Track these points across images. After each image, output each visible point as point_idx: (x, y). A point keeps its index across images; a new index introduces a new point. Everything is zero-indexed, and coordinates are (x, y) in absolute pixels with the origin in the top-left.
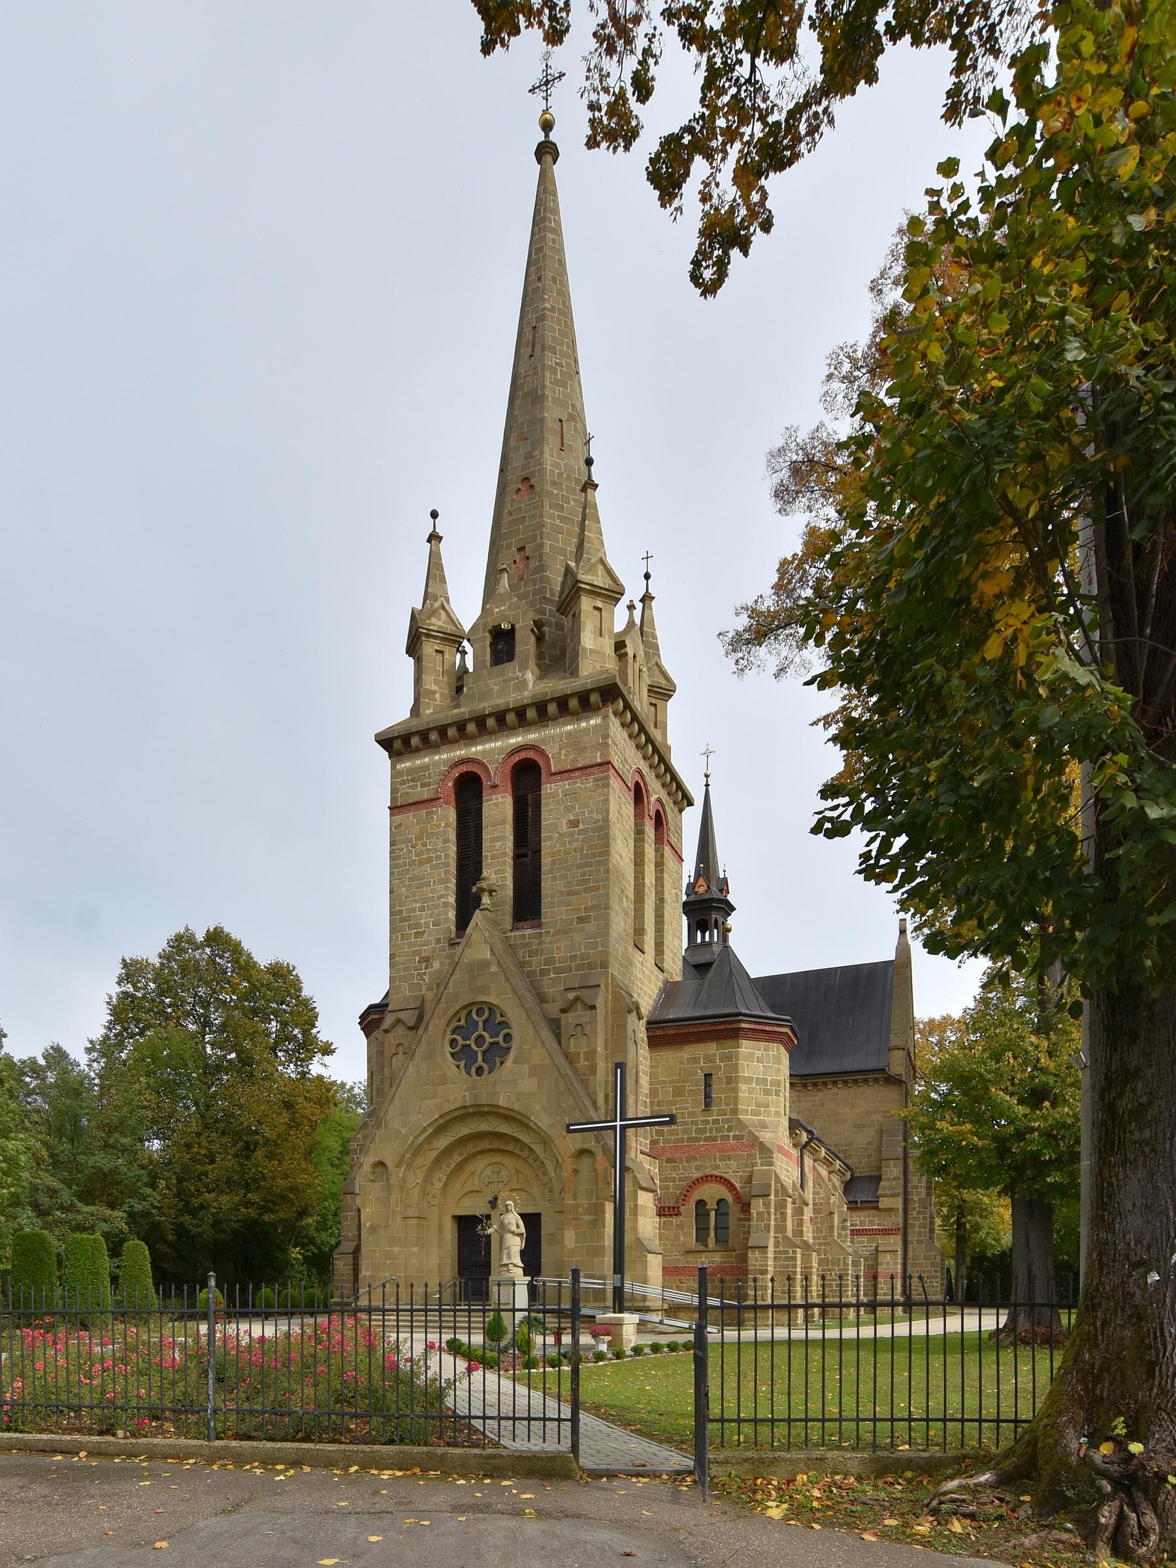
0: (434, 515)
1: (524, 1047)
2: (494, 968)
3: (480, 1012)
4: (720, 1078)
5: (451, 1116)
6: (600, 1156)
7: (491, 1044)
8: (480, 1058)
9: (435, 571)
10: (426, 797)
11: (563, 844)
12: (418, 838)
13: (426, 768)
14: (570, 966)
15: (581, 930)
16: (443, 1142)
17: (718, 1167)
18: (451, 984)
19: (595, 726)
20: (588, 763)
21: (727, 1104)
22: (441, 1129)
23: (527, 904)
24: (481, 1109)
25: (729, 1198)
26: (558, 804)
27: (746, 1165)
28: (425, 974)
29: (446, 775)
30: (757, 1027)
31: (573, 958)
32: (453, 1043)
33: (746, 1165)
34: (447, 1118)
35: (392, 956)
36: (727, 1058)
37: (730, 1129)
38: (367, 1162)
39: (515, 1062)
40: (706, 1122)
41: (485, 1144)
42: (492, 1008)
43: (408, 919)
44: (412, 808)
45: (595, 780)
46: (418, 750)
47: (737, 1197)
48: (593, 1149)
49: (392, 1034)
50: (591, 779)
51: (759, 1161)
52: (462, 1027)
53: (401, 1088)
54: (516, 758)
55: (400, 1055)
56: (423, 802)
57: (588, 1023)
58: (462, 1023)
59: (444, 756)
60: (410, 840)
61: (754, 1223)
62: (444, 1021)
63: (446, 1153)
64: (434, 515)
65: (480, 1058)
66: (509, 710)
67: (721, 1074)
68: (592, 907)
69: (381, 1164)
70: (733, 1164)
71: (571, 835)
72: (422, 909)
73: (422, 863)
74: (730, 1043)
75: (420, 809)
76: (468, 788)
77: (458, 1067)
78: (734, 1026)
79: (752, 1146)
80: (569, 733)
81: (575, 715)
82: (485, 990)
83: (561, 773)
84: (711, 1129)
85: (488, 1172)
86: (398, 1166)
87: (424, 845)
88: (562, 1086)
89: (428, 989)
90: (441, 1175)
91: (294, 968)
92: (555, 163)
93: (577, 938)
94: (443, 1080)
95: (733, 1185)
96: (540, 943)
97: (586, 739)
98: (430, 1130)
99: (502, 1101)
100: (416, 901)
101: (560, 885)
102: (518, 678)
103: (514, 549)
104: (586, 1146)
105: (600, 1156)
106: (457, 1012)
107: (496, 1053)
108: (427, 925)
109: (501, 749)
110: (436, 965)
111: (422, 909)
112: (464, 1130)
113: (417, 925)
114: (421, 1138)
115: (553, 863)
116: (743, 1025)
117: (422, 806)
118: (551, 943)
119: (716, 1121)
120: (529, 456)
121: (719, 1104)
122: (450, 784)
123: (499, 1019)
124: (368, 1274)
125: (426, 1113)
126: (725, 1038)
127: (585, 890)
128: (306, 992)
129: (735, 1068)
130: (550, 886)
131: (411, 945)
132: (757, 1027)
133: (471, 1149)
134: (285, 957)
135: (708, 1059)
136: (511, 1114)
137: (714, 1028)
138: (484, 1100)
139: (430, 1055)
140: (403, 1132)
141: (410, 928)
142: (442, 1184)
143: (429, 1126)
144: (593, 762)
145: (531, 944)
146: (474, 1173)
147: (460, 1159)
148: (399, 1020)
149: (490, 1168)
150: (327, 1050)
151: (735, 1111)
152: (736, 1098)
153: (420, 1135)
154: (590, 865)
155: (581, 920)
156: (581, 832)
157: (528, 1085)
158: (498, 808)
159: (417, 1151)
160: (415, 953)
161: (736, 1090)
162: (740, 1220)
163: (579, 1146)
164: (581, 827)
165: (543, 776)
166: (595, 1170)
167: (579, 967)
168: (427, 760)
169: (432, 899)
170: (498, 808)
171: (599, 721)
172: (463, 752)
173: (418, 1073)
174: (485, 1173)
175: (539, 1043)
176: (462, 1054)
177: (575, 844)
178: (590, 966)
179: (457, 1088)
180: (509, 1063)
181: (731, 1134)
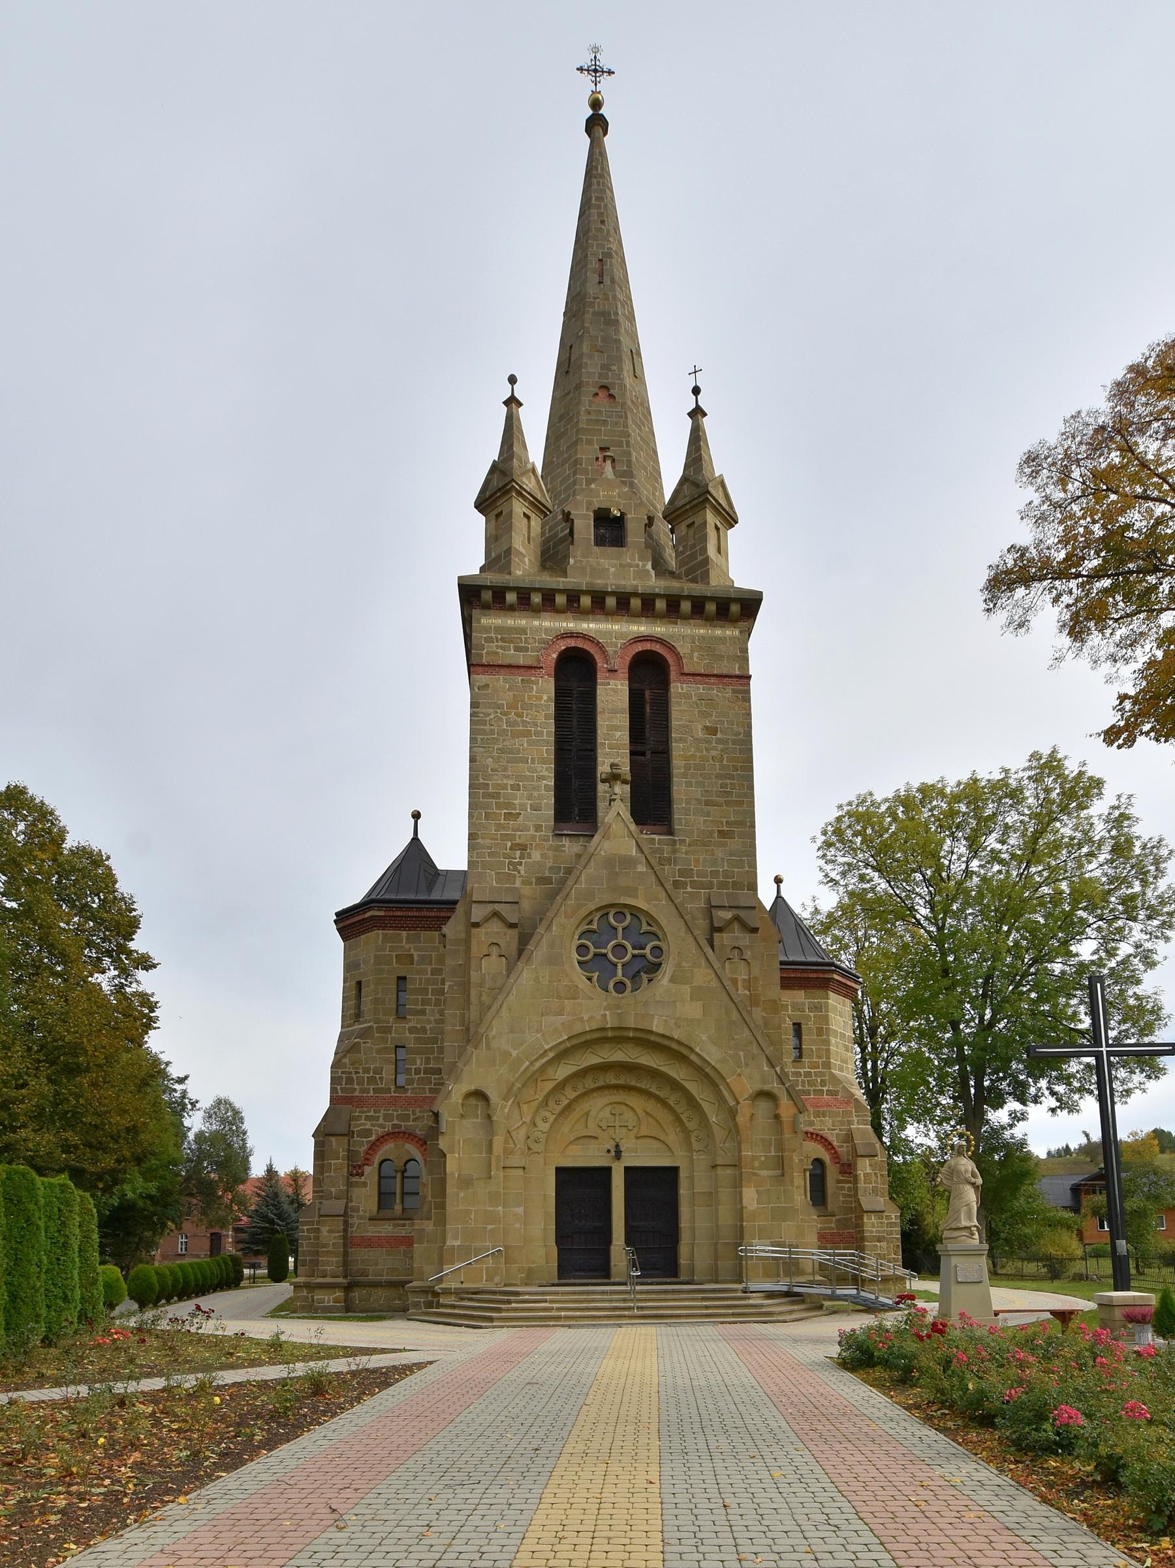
0: (512, 380)
1: (684, 964)
2: (642, 868)
3: (620, 915)
4: (810, 1029)
5: (583, 1039)
6: (784, 1100)
7: (634, 956)
8: (620, 972)
9: (512, 432)
10: (521, 662)
11: (698, 749)
12: (510, 706)
13: (523, 631)
14: (711, 883)
15: (724, 845)
16: (563, 1071)
17: (812, 1123)
18: (583, 877)
19: (732, 638)
20: (725, 672)
21: (819, 1057)
22: (563, 1054)
23: (652, 804)
24: (626, 1034)
25: (827, 1158)
26: (691, 706)
27: (842, 1123)
28: (521, 864)
29: (549, 645)
30: (843, 980)
31: (714, 874)
32: (582, 950)
33: (842, 1123)
34: (575, 1042)
35: (472, 837)
36: (817, 1008)
37: (823, 1083)
38: (457, 1090)
39: (673, 980)
40: (798, 1074)
41: (611, 1079)
42: (636, 912)
43: (496, 796)
44: (502, 670)
45: (734, 691)
46: (512, 608)
47: (836, 1156)
48: (775, 1091)
49: (482, 930)
50: (729, 689)
51: (855, 1119)
52: (594, 932)
53: (511, 997)
54: (640, 647)
55: (494, 957)
56: (519, 667)
57: (747, 947)
58: (595, 926)
59: (546, 624)
60: (500, 707)
61: (861, 1185)
62: (574, 921)
63: (561, 1086)
64: (512, 380)
65: (620, 972)
66: (635, 594)
67: (811, 1024)
68: (736, 823)
69: (479, 1095)
70: (829, 1121)
71: (708, 742)
72: (515, 787)
73: (516, 735)
74: (819, 992)
75: (513, 674)
76: (576, 669)
77: (590, 979)
78: (826, 976)
79: (848, 1103)
80: (703, 638)
81: (709, 620)
82: (632, 891)
83: (694, 675)
84: (803, 1082)
85: (606, 1113)
86: (506, 1099)
87: (520, 715)
88: (735, 1015)
89: (523, 882)
90: (548, 1114)
91: (108, 858)
92: (605, 133)
93: (719, 853)
94: (573, 993)
95: (830, 1144)
96: (674, 851)
97: (722, 647)
98: (551, 1055)
99: (657, 1026)
100: (507, 777)
101: (697, 792)
102: (638, 566)
103: (597, 447)
104: (766, 1087)
105: (784, 1100)
106: (591, 913)
107: (647, 968)
108: (523, 807)
109: (619, 635)
110: (536, 856)
111: (515, 787)
112: (591, 1059)
113: (508, 805)
114: (538, 1065)
115: (688, 767)
116: (836, 977)
117: (515, 671)
118: (686, 853)
119: (808, 1074)
120: (606, 367)
121: (811, 1056)
122: (555, 656)
123: (645, 928)
124: (457, 1243)
125: (551, 1031)
126: (815, 987)
127: (727, 803)
128: (124, 887)
129: (826, 1019)
130: (682, 790)
131: (499, 827)
132: (843, 980)
133: (589, 1083)
134: (97, 843)
135: (797, 1007)
136: (666, 1042)
137: (806, 975)
138: (631, 1023)
139: (553, 960)
140: (514, 1053)
141: (499, 806)
142: (547, 1125)
143: (551, 1049)
144: (732, 672)
145: (661, 851)
146: (587, 1114)
147: (574, 1094)
148: (496, 914)
149: (608, 1109)
150: (146, 963)
151: (827, 1065)
152: (828, 1051)
153: (536, 1060)
154: (731, 777)
155: (722, 834)
156: (720, 741)
157: (692, 1010)
158: (613, 696)
159: (533, 1079)
160: (505, 837)
161: (828, 1042)
162: (839, 1181)
163: (758, 1086)
164: (719, 735)
165: (673, 675)
166: (777, 1117)
167: (723, 885)
168: (524, 622)
169: (531, 779)
170: (613, 696)
171: (736, 633)
172: (571, 625)
173: (537, 980)
174: (601, 1115)
175: (703, 961)
176: (595, 964)
177: (713, 753)
178: (736, 885)
179: (594, 1008)
180: (665, 981)
181: (825, 1089)
